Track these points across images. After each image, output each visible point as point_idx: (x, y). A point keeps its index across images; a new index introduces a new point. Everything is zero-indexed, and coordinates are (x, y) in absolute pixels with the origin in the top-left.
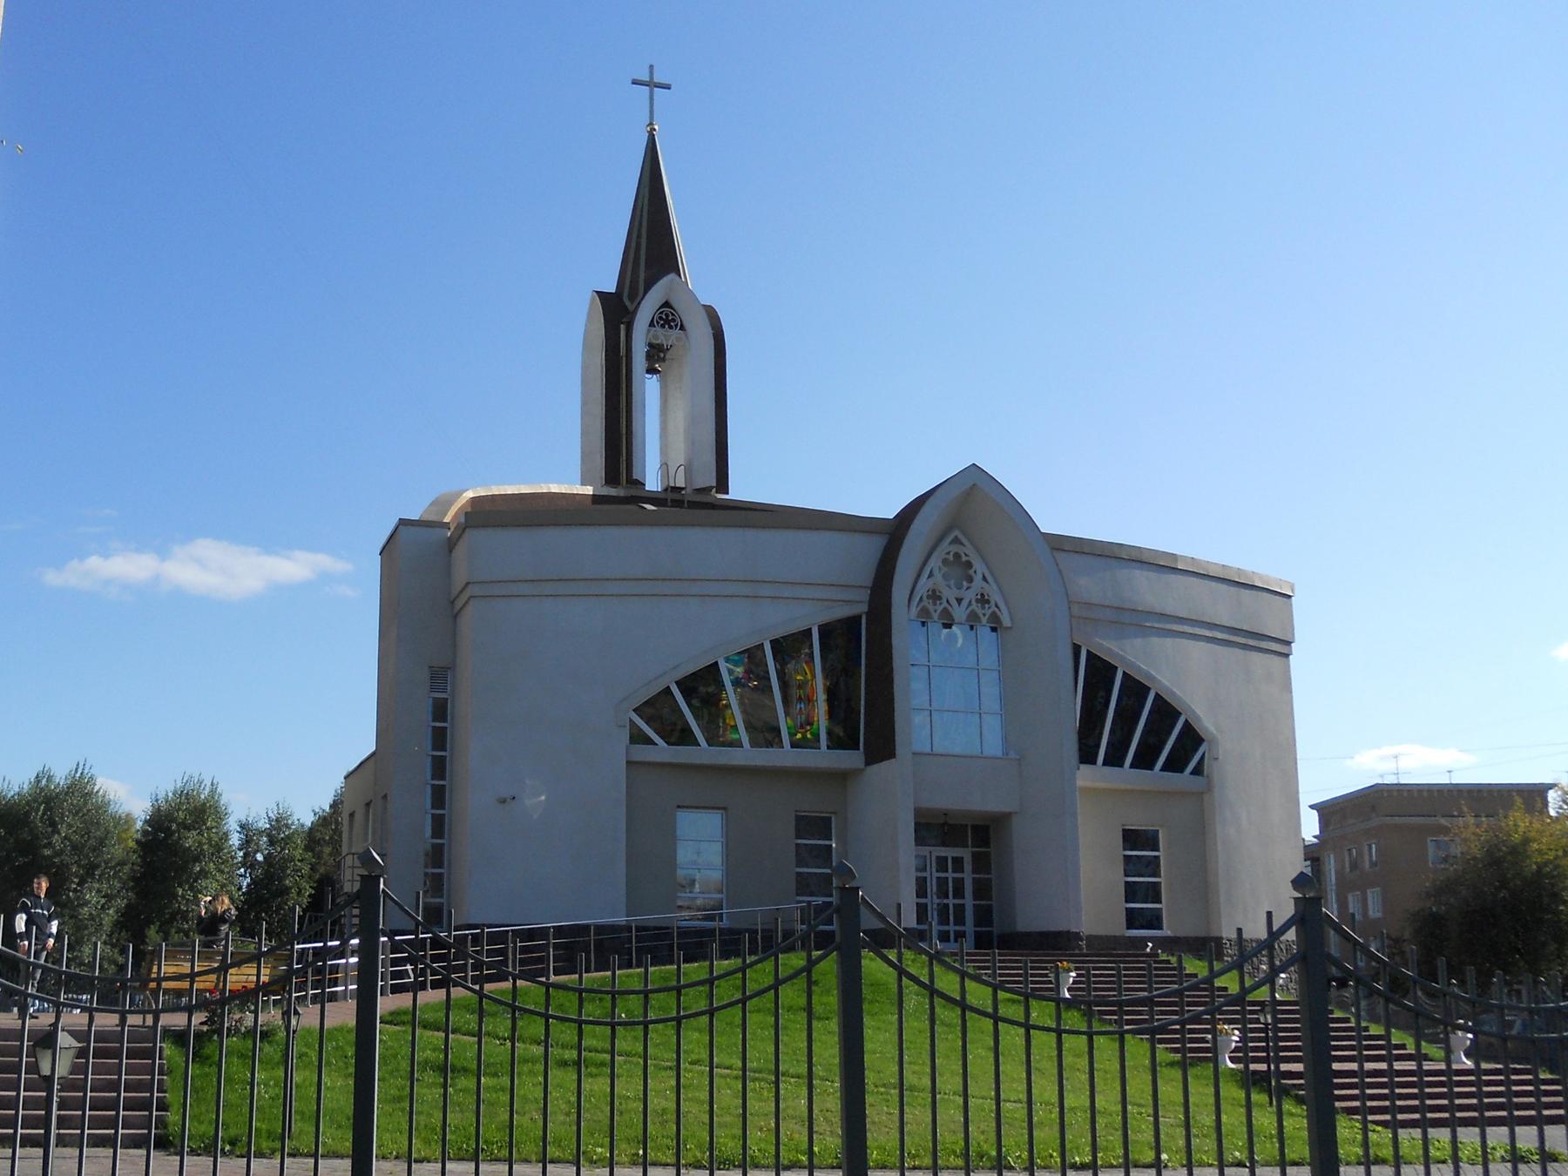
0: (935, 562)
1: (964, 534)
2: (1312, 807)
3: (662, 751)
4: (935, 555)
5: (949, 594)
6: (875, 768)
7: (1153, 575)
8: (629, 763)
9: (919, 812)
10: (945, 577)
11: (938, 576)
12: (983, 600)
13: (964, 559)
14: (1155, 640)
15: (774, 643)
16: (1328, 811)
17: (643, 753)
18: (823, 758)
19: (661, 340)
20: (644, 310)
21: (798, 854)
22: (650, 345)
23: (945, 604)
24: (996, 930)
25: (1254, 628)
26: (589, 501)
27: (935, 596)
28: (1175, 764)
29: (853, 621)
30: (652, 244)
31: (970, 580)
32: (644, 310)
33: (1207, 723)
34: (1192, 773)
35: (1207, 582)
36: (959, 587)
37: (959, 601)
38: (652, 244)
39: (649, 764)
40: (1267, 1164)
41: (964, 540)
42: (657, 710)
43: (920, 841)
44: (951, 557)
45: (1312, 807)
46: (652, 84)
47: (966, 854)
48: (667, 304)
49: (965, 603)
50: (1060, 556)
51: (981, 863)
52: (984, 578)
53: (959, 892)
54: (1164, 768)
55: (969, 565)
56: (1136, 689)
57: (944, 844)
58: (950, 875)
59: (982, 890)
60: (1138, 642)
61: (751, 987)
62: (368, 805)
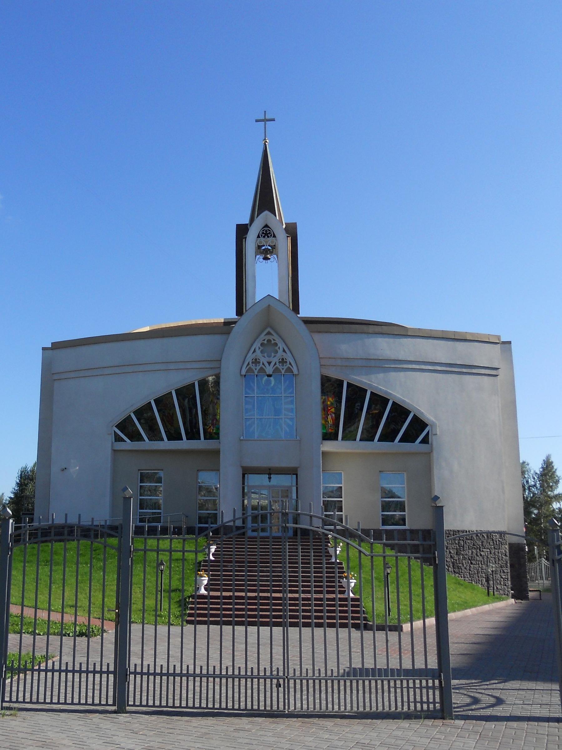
0: (257, 345)
1: (272, 328)
3: (128, 444)
4: (258, 340)
5: (263, 360)
7: (391, 340)
10: (262, 352)
11: (258, 352)
12: (283, 361)
13: (273, 342)
14: (393, 374)
15: (177, 391)
20: (263, 228)
23: (288, 365)
25: (479, 361)
26: (222, 325)
27: (256, 362)
28: (408, 438)
30: (264, 199)
31: (276, 352)
32: (263, 228)
33: (427, 415)
34: (420, 443)
35: (430, 341)
36: (269, 356)
37: (269, 363)
38: (264, 199)
39: (123, 451)
40: (54, 634)
41: (272, 332)
42: (125, 426)
44: (265, 342)
48: (266, 226)
49: (272, 364)
52: (284, 351)
54: (402, 440)
56: (379, 400)
60: (381, 375)
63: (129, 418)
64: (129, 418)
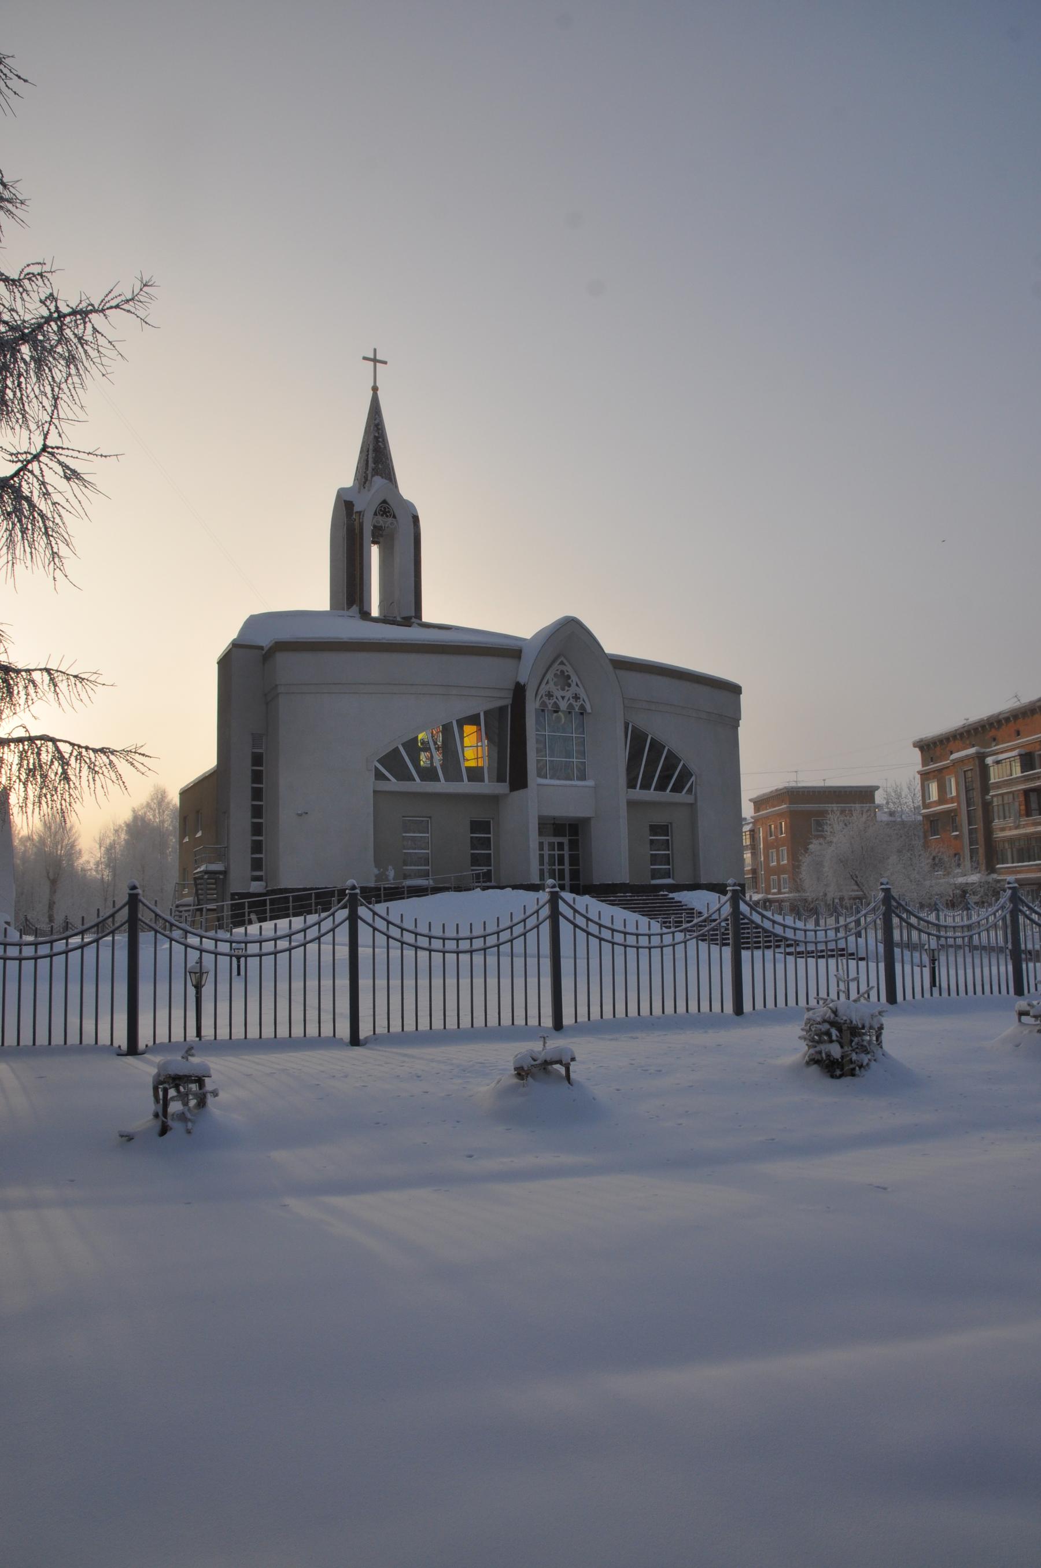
0: (550, 676)
2: (750, 800)
3: (393, 784)
5: (558, 693)
6: (516, 793)
8: (375, 792)
9: (540, 818)
11: (551, 683)
12: (576, 697)
16: (759, 803)
17: (383, 786)
18: (487, 787)
19: (381, 523)
21: (472, 842)
22: (375, 527)
24: (582, 883)
28: (677, 788)
29: (502, 710)
31: (569, 685)
33: (693, 767)
41: (565, 661)
43: (541, 834)
45: (750, 800)
46: (375, 360)
47: (565, 840)
48: (385, 502)
50: (621, 673)
51: (574, 845)
53: (561, 862)
55: (569, 677)
56: (657, 747)
57: (555, 835)
58: (556, 852)
59: (574, 860)
61: (515, 935)
62: (198, 812)
63: (396, 750)
64: (396, 750)
